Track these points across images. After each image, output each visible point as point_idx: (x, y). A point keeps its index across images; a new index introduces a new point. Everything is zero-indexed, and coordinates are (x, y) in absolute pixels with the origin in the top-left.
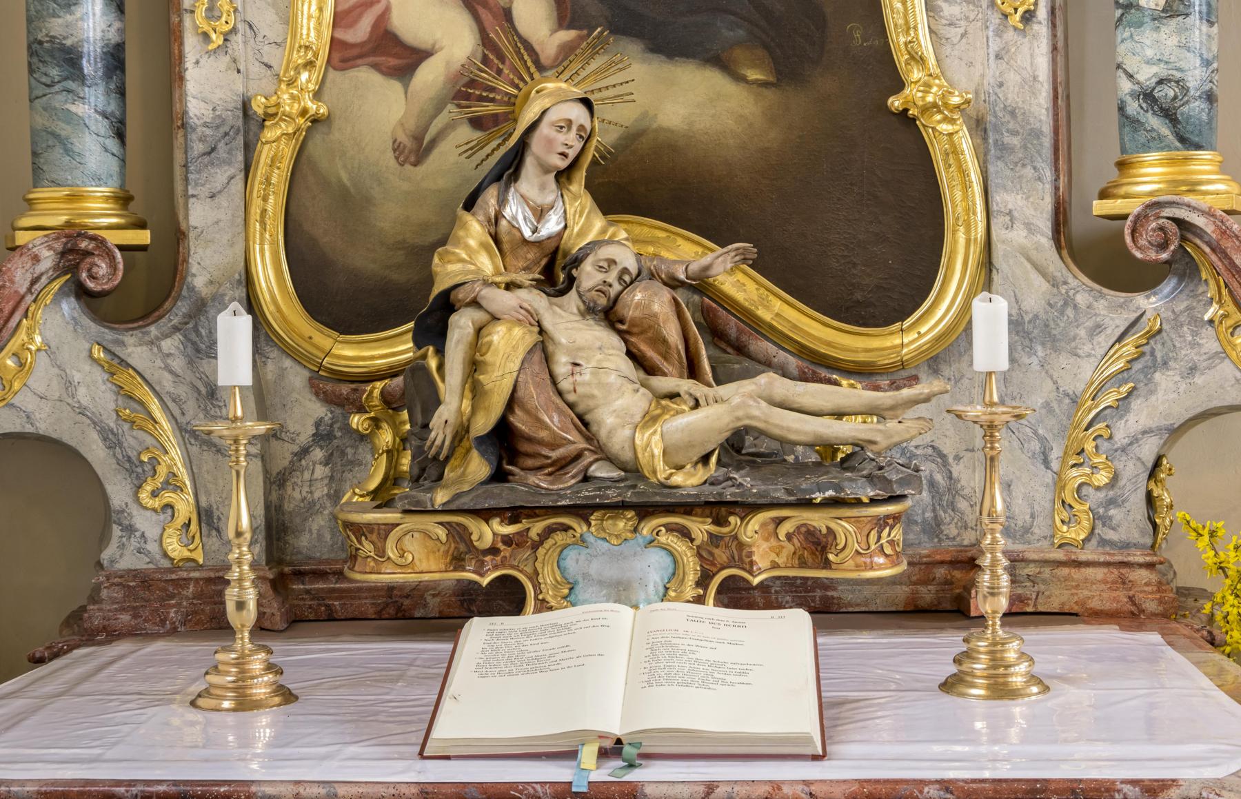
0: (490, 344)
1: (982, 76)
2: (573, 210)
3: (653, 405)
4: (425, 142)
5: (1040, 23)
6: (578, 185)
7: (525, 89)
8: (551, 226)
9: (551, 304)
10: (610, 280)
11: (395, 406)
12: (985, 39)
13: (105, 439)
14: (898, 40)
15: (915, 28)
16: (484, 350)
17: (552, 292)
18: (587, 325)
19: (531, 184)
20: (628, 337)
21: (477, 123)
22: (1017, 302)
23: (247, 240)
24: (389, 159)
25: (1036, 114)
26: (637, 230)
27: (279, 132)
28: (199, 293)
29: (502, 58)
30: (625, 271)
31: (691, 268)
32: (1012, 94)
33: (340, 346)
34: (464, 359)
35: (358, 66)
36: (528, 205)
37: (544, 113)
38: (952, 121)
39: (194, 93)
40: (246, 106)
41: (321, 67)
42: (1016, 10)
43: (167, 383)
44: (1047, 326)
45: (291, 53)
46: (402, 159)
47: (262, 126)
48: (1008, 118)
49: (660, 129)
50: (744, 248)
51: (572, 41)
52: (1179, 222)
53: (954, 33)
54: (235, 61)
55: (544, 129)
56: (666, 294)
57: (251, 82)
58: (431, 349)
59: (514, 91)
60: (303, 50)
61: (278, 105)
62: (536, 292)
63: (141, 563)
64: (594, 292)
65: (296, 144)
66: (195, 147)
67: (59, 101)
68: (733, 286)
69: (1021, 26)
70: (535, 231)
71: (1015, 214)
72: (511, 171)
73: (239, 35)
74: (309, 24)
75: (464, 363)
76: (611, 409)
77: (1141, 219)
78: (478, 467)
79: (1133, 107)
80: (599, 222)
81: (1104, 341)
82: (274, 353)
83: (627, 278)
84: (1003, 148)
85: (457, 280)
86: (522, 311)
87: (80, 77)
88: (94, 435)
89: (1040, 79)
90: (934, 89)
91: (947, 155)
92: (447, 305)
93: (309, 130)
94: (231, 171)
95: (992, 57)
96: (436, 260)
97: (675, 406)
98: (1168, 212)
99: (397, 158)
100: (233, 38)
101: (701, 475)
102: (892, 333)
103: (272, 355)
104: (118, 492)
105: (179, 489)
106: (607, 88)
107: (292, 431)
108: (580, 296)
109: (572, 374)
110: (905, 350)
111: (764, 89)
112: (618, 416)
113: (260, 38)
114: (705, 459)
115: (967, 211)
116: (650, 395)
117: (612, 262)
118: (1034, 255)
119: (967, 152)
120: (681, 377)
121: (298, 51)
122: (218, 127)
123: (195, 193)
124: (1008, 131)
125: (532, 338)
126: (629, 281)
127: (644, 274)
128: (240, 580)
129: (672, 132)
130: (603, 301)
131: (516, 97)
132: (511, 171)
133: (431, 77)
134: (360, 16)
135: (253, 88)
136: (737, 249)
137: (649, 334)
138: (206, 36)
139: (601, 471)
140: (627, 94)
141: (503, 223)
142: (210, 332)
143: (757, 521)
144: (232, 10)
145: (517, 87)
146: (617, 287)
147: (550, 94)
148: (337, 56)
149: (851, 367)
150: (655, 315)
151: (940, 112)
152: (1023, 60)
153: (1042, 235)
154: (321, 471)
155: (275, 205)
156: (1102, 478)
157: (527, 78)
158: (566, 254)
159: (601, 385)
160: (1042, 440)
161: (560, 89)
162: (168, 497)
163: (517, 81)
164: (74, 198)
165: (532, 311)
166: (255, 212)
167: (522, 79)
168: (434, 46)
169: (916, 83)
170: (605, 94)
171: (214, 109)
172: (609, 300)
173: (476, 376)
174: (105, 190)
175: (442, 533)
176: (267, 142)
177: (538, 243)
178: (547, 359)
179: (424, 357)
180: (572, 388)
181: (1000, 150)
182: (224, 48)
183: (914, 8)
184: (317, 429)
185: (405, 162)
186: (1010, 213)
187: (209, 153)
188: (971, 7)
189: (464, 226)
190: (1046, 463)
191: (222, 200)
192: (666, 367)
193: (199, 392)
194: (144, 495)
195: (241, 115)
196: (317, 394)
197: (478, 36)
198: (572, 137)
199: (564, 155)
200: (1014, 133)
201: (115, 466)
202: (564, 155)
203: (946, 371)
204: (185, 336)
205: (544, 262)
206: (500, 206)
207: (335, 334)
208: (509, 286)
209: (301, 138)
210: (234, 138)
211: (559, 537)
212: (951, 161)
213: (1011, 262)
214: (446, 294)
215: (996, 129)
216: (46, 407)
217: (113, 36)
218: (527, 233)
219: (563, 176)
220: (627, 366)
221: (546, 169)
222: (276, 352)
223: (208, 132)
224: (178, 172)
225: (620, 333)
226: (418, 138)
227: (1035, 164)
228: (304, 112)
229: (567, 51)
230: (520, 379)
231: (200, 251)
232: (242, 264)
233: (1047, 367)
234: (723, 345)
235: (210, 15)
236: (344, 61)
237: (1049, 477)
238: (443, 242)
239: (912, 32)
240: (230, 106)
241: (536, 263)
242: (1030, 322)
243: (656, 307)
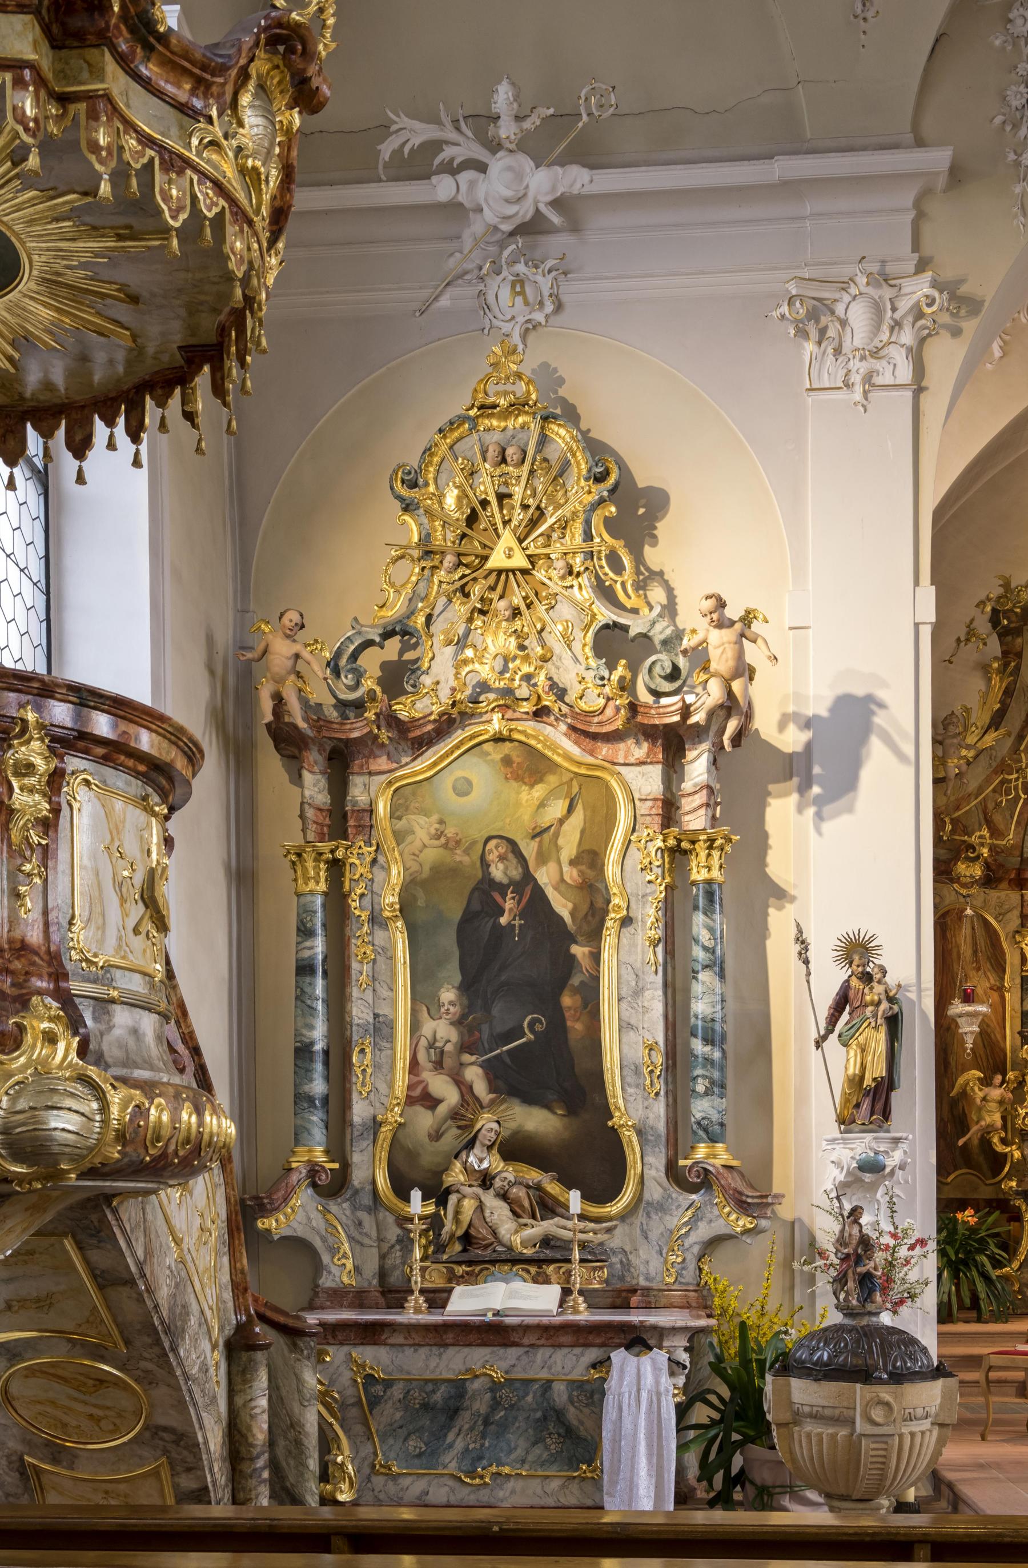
6: (495, 1151)
8: (485, 1165)
14: (611, 1101)
19: (478, 1150)
21: (459, 1127)
24: (427, 1140)
29: (468, 1105)
32: (651, 1122)
40: (375, 1118)
43: (344, 1219)
47: (380, 1125)
52: (705, 1169)
53: (632, 1099)
55: (483, 1131)
56: (524, 1190)
63: (332, 1285)
67: (306, 1115)
77: (691, 1167)
78: (458, 1247)
79: (695, 1127)
80: (502, 1164)
81: (681, 1210)
82: (382, 1210)
87: (315, 1107)
92: (448, 1192)
98: (701, 1165)
101: (533, 1250)
104: (326, 1258)
105: (347, 1258)
114: (535, 1246)
125: (477, 1204)
126: (511, 1185)
127: (517, 1183)
130: (502, 1192)
138: (361, 1093)
139: (499, 1248)
143: (551, 1268)
152: (655, 1109)
154: (398, 1254)
155: (384, 1155)
156: (679, 1260)
159: (501, 1220)
160: (660, 1246)
162: (344, 1261)
164: (310, 1151)
166: (377, 1158)
174: (321, 1148)
175: (445, 1270)
177: (480, 1171)
189: (454, 1164)
190: (661, 1254)
191: (365, 1153)
192: (524, 1215)
194: (335, 1260)
198: (493, 1135)
203: (628, 1221)
208: (470, 1186)
211: (485, 1272)
214: (448, 1188)
216: (301, 1227)
217: (326, 1092)
218: (476, 1167)
219: (490, 1148)
220: (510, 1214)
221: (483, 1145)
224: (348, 1142)
225: (509, 1203)
226: (437, 1132)
229: (492, 1102)
237: (662, 1259)
238: (446, 1169)
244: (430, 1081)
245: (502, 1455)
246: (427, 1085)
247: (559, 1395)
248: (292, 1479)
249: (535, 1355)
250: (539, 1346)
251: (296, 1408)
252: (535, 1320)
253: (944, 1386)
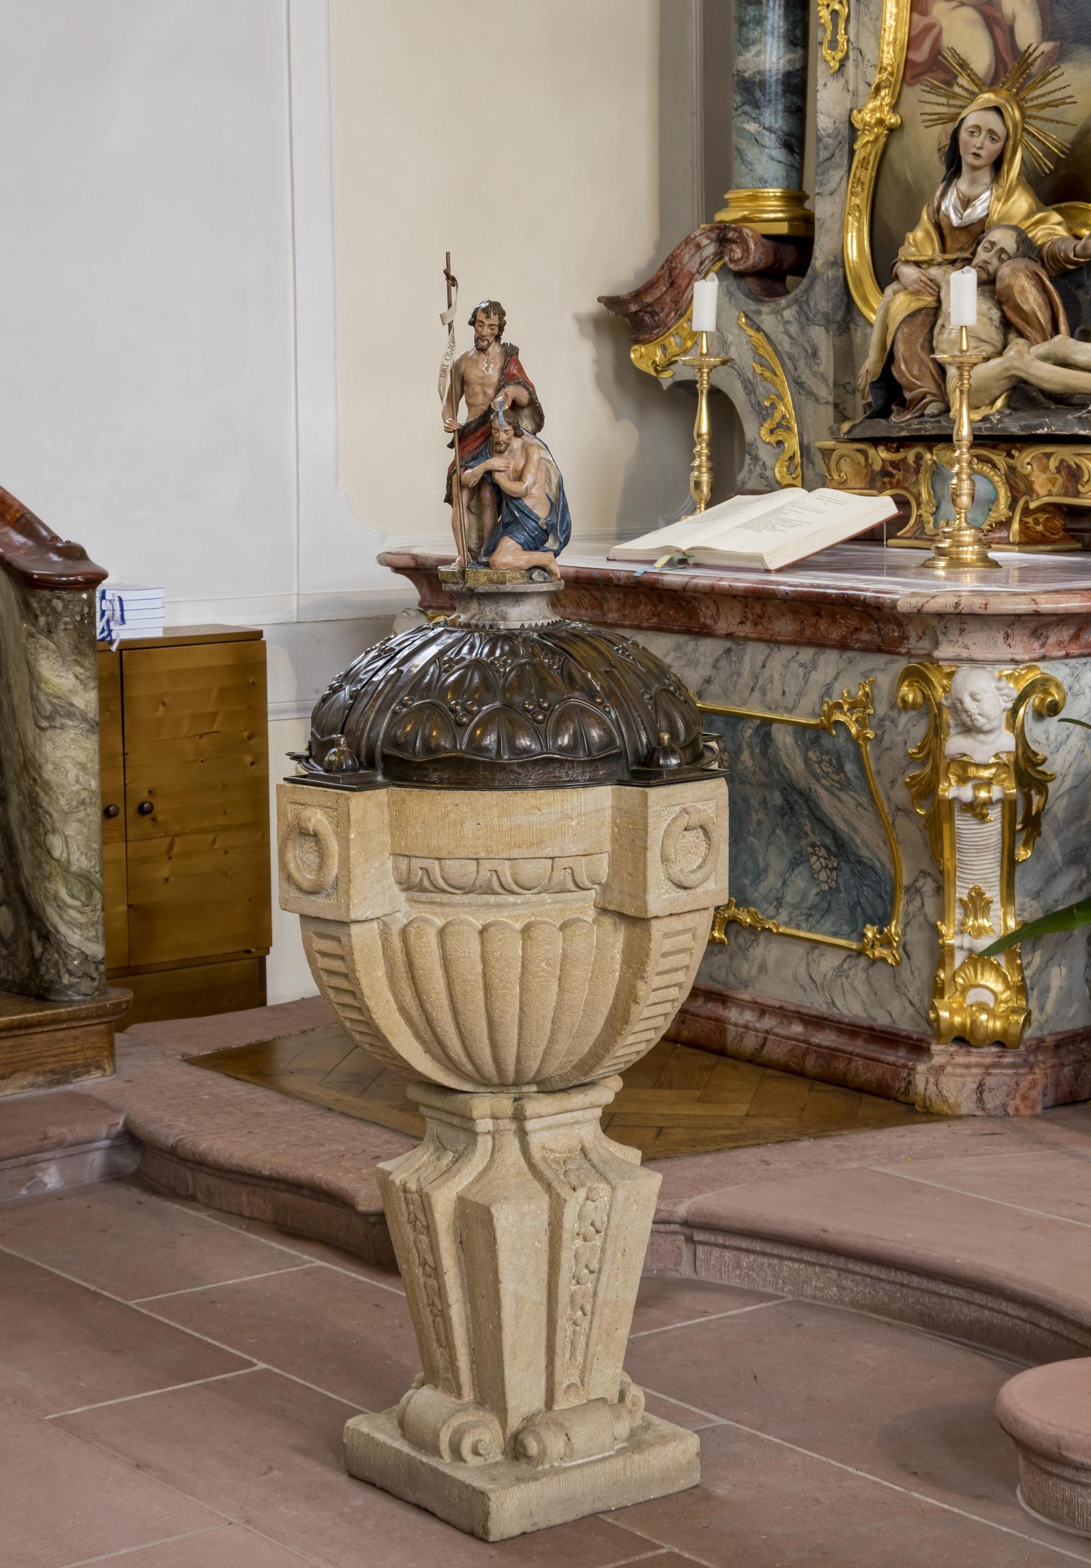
8: (977, 211)
13: (745, 387)
30: (1002, 250)
88: (738, 384)
113: (866, 62)
122: (836, 137)
128: (700, 466)
134: (925, 37)
162: (781, 435)
168: (997, 183)
174: (778, 192)
177: (965, 229)
193: (807, 352)
194: (763, 432)
201: (750, 409)
204: (800, 307)
223: (830, 141)
244: (945, 23)
245: (747, 882)
246: (940, 33)
247: (788, 755)
248: (27, 872)
249: (741, 660)
250: (746, 639)
251: (31, 733)
252: (744, 581)
253: (618, 809)
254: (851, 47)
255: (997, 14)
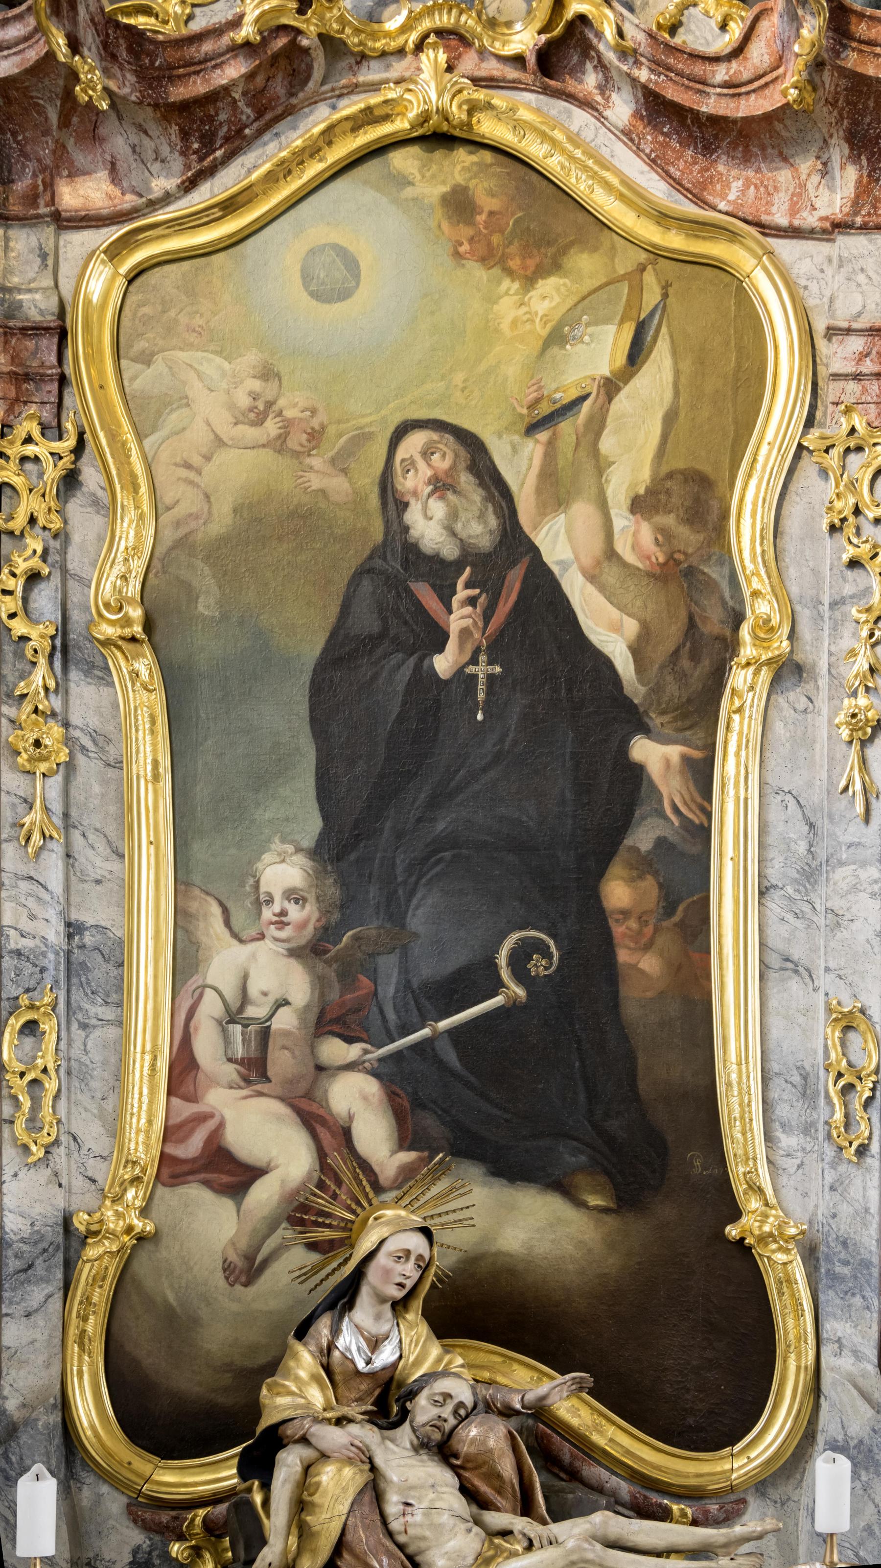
0: (318, 1484)
1: (816, 1206)
2: (408, 1340)
3: (486, 1545)
4: (257, 1262)
5: (873, 1156)
6: (414, 1315)
7: (362, 1214)
8: (386, 1356)
9: (384, 1438)
10: (444, 1415)
11: (218, 1533)
12: (820, 1171)
14: (737, 1171)
15: (755, 1159)
16: (312, 1490)
17: (385, 1425)
18: (422, 1461)
20: (461, 1472)
22: (843, 1428)
23: (64, 1361)
25: (867, 1245)
26: (473, 1356)
27: (101, 1250)
28: (11, 1416)
29: (339, 1183)
30: (461, 1404)
31: (527, 1397)
33: (161, 1472)
34: (291, 1499)
35: (188, 1182)
36: (362, 1335)
37: (382, 1242)
38: (787, 1251)
39: (12, 1207)
40: (67, 1222)
41: (148, 1183)
42: (851, 1143)
44: (870, 1451)
45: (117, 1169)
46: (232, 1279)
48: (840, 1248)
49: (499, 1254)
50: (581, 1378)
51: (412, 1163)
53: (790, 1164)
54: (56, 1174)
55: (381, 1259)
57: (74, 1197)
58: (256, 1483)
59: (349, 1216)
60: (130, 1165)
61: (101, 1222)
62: (369, 1426)
64: (428, 1428)
65: (119, 1262)
66: (11, 1264)
68: (568, 1411)
69: (855, 1159)
70: (369, 1362)
71: (844, 1341)
72: (345, 1300)
73: (62, 1148)
74: (137, 1139)
75: (290, 1503)
76: (443, 1551)
80: (435, 1350)
82: (89, 1479)
83: (462, 1412)
84: (835, 1278)
85: (286, 1415)
86: (353, 1449)
89: (872, 1211)
90: (771, 1220)
91: (781, 1283)
93: (134, 1247)
94: (49, 1289)
95: (827, 1189)
96: (264, 1391)
97: (508, 1546)
99: (227, 1278)
100: (55, 1150)
102: (722, 1458)
103: (88, 1481)
106: (447, 1213)
107: (108, 1558)
108: (414, 1431)
109: (404, 1514)
110: (734, 1476)
111: (604, 1215)
112: (449, 1559)
113: (84, 1151)
115: (798, 1339)
116: (483, 1534)
117: (447, 1396)
118: (860, 1381)
119: (799, 1281)
120: (515, 1513)
121: (125, 1167)
122: (36, 1243)
123: (9, 1311)
124: (839, 1261)
126: (464, 1415)
129: (511, 1256)
130: (437, 1436)
131: (353, 1222)
132: (345, 1300)
133: (265, 1196)
135: (76, 1202)
136: (574, 1379)
137: (484, 1470)
138: (26, 1148)
140: (467, 1219)
141: (336, 1354)
142: (21, 1459)
144: (55, 1122)
145: (353, 1212)
146: (452, 1421)
147: (387, 1223)
148: (166, 1172)
149: (681, 1491)
150: (491, 1451)
151: (775, 1241)
152: (855, 1191)
153: (869, 1362)
155: (94, 1326)
157: (365, 1204)
158: (400, 1385)
159: (433, 1526)
161: (399, 1217)
163: (354, 1206)
165: (364, 1448)
166: (73, 1332)
167: (359, 1203)
168: (269, 1164)
169: (753, 1212)
170: (444, 1219)
171: (32, 1225)
172: (443, 1435)
173: (303, 1516)
176: (88, 1261)
177: (372, 1375)
178: (378, 1498)
179: (249, 1490)
180: (403, 1529)
181: (832, 1279)
182: (45, 1160)
183: (753, 1139)
184: (134, 1556)
185: (235, 1282)
186: (839, 1341)
187: (25, 1270)
188: (808, 1139)
189: (295, 1356)
191: (39, 1320)
192: (500, 1501)
195: (61, 1231)
196: (135, 1521)
197: (315, 1155)
199: (401, 1285)
200: (846, 1263)
202: (401, 1285)
205: (377, 1393)
206: (333, 1337)
207: (156, 1459)
208: (340, 1422)
209: (126, 1256)
210: (53, 1255)
212: (785, 1290)
213: (839, 1389)
214: (273, 1429)
215: (828, 1259)
218: (361, 1365)
219: (399, 1306)
222: (92, 1477)
223: (25, 1248)
225: (454, 1468)
226: (250, 1258)
227: (865, 1293)
228: (129, 1229)
229: (407, 1173)
230: (349, 1523)
231: (13, 1373)
232: (58, 1386)
233: (870, 1491)
234: (556, 1471)
235: (31, 1125)
236: (174, 1176)
239: (751, 1163)
240: (50, 1222)
241: (369, 1393)
242: (855, 1448)
243: (492, 1443)
244: (229, 1115)
246: (221, 1125)
254: (62, 1131)
255: (321, 1112)
